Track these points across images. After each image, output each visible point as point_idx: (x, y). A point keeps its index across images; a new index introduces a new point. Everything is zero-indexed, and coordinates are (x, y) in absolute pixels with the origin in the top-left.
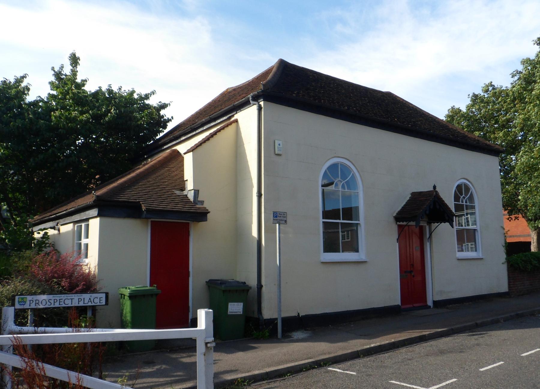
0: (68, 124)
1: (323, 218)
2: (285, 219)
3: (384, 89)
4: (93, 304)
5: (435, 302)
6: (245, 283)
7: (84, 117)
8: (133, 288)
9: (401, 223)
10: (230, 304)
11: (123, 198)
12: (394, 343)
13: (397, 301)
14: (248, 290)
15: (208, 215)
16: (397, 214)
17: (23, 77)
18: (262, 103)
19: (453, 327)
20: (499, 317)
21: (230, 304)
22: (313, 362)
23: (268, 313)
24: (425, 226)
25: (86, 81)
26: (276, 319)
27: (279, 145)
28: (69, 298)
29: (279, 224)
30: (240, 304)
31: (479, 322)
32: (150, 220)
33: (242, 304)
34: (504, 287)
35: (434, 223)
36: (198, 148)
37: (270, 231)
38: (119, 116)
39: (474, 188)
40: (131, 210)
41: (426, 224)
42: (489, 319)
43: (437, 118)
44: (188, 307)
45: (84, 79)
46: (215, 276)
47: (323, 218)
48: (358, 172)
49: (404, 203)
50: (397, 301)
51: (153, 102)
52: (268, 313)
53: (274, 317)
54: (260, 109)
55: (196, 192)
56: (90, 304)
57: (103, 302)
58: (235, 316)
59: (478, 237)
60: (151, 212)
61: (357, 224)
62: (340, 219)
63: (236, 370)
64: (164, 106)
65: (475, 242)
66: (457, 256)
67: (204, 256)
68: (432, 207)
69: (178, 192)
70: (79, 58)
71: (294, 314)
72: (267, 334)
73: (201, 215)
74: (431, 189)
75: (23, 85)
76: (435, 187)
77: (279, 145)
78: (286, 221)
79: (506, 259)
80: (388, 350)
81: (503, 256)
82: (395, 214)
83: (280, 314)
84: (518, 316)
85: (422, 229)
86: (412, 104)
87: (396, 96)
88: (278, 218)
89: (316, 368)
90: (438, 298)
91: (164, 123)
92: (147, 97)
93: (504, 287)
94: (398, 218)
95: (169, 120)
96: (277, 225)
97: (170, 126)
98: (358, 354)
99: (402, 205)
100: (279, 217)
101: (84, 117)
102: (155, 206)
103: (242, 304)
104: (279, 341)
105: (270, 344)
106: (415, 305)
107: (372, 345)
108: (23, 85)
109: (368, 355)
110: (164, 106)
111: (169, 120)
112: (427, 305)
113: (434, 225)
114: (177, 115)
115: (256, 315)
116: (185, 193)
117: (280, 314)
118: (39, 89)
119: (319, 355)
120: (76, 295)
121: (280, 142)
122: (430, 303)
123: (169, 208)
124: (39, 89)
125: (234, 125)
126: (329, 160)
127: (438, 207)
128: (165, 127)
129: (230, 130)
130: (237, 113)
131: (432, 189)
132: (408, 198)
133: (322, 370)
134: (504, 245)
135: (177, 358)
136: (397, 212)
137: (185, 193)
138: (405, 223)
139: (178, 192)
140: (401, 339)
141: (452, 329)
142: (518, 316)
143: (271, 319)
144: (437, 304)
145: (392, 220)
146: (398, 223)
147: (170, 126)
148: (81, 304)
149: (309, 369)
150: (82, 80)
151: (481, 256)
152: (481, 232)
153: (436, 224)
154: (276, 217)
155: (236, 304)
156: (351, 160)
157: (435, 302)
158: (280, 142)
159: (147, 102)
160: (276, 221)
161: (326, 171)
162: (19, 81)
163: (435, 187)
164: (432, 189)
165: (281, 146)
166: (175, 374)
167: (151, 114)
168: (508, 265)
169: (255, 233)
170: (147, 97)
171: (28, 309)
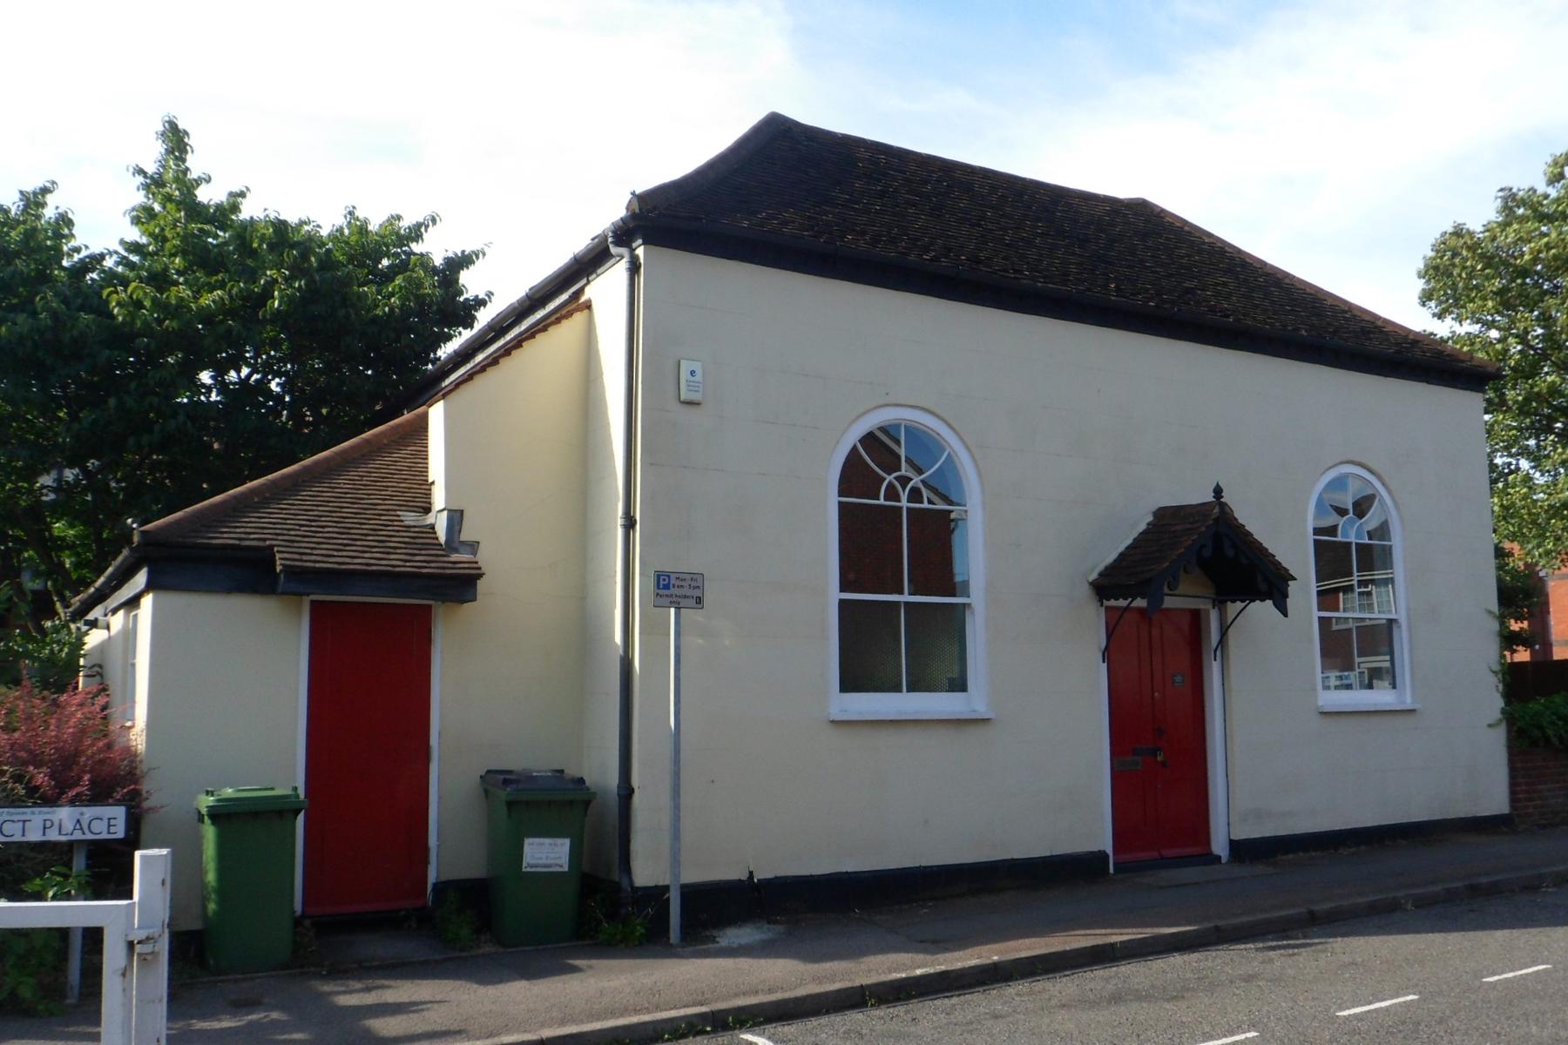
0: (160, 322)
1: (842, 590)
2: (697, 593)
3: (1120, 187)
4: (89, 836)
5: (1235, 846)
6: (581, 781)
7: (207, 300)
8: (229, 792)
9: (1112, 603)
10: (527, 841)
11: (226, 537)
12: (995, 965)
13: (1100, 838)
14: (587, 803)
15: (480, 583)
16: (1101, 575)
17: (45, 191)
18: (640, 252)
19: (1220, 923)
20: (1401, 894)
21: (527, 841)
22: (702, 1016)
23: (646, 871)
24: (1207, 612)
25: (242, 195)
26: (666, 888)
27: (692, 373)
28: (15, 818)
29: (678, 609)
30: (559, 841)
31: (1320, 907)
32: (306, 601)
33: (567, 842)
34: (1494, 798)
35: (1233, 601)
36: (462, 387)
37: (654, 629)
38: (312, 295)
39: (1389, 492)
40: (250, 572)
41: (1209, 606)
42: (1360, 900)
43: (1287, 275)
44: (426, 849)
45: (236, 189)
46: (514, 761)
47: (842, 590)
48: (967, 448)
49: (1129, 541)
50: (1100, 838)
51: (436, 247)
52: (646, 871)
53: (667, 882)
54: (634, 268)
55: (456, 518)
56: (78, 836)
57: (119, 832)
58: (548, 879)
59: (1402, 639)
60: (302, 579)
61: (964, 605)
62: (901, 592)
63: (459, 1032)
64: (465, 261)
65: (1391, 653)
66: (1320, 703)
67: (479, 702)
68: (1207, 553)
69: (409, 518)
70: (186, 133)
71: (737, 874)
72: (640, 930)
73: (461, 585)
74: (1209, 497)
75: (49, 213)
76: (1218, 491)
77: (692, 373)
78: (699, 600)
79: (1503, 712)
80: (971, 986)
81: (1494, 703)
82: (1094, 576)
83: (676, 874)
84: (1475, 891)
85: (1196, 618)
86: (1210, 235)
87: (1163, 210)
88: (673, 591)
89: (704, 1032)
90: (1242, 833)
91: (464, 314)
92: (416, 233)
93: (1494, 798)
94: (1106, 586)
95: (480, 303)
96: (673, 610)
97: (484, 317)
98: (864, 995)
99: (1121, 548)
100: (674, 589)
101: (207, 300)
102: (320, 557)
103: (567, 842)
104: (669, 951)
105: (638, 961)
106: (1167, 853)
107: (919, 972)
108: (49, 213)
109: (898, 999)
110: (465, 261)
111: (480, 303)
112: (1210, 853)
113: (1233, 608)
114: (496, 285)
115: (615, 876)
116: (430, 519)
117: (676, 875)
118: (103, 226)
119: (736, 995)
120: (37, 810)
121: (697, 366)
122: (1219, 846)
123: (357, 564)
124: (103, 226)
125: (579, 318)
126: (859, 417)
127: (1230, 553)
128: (468, 322)
129: (569, 329)
130: (588, 282)
131: (1210, 498)
132: (1142, 527)
133: (724, 1039)
134: (1497, 667)
135: (330, 994)
136: (1101, 567)
137: (430, 519)
138: (1122, 603)
139: (409, 518)
140: (1023, 954)
141: (1217, 928)
142: (1475, 891)
143: (656, 887)
144: (1242, 850)
145: (1085, 591)
146: (1106, 603)
147: (484, 317)
148: (53, 836)
149: (684, 1036)
150: (231, 195)
151: (1408, 702)
152: (1410, 629)
153: (1239, 605)
154: (667, 587)
155: (547, 841)
156: (938, 411)
157: (1235, 846)
158: (697, 366)
159: (416, 248)
160: (666, 601)
161: (854, 448)
162: (34, 201)
163: (1218, 491)
164: (1210, 498)
165: (698, 377)
166: (80, 1029)
167: (430, 287)
168: (1509, 732)
169: (618, 638)
170: (416, 233)
171: (70, 845)
